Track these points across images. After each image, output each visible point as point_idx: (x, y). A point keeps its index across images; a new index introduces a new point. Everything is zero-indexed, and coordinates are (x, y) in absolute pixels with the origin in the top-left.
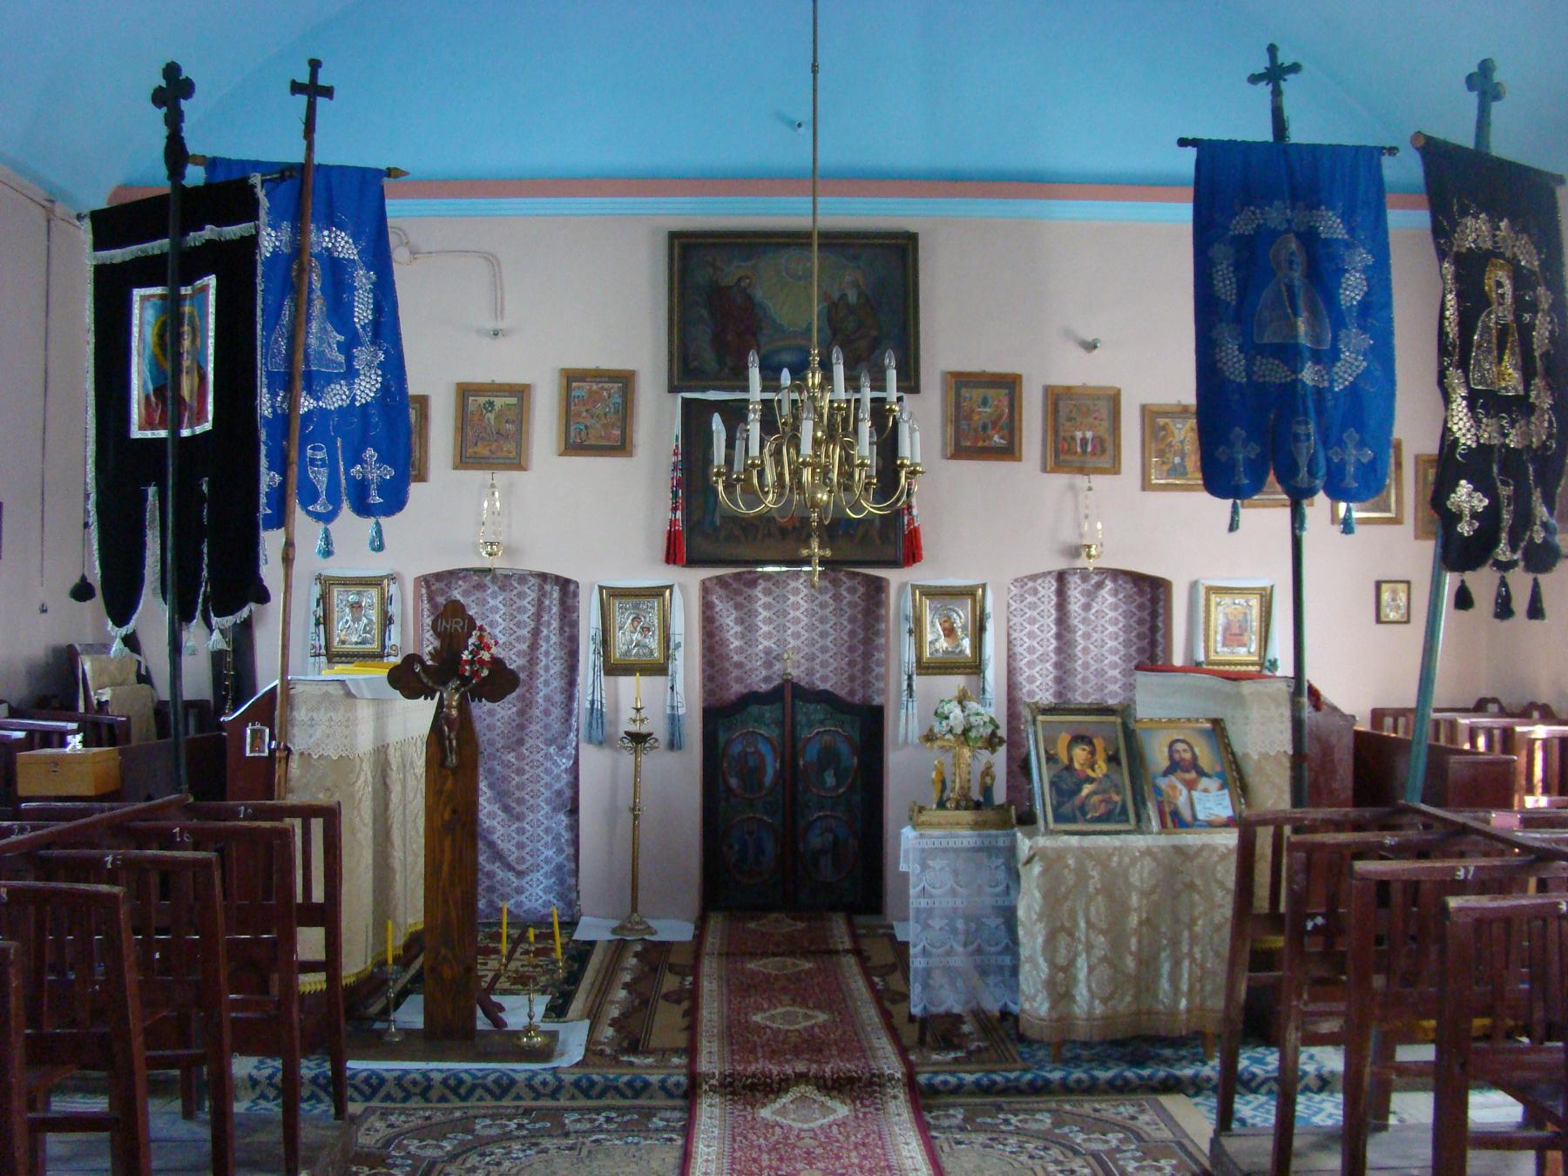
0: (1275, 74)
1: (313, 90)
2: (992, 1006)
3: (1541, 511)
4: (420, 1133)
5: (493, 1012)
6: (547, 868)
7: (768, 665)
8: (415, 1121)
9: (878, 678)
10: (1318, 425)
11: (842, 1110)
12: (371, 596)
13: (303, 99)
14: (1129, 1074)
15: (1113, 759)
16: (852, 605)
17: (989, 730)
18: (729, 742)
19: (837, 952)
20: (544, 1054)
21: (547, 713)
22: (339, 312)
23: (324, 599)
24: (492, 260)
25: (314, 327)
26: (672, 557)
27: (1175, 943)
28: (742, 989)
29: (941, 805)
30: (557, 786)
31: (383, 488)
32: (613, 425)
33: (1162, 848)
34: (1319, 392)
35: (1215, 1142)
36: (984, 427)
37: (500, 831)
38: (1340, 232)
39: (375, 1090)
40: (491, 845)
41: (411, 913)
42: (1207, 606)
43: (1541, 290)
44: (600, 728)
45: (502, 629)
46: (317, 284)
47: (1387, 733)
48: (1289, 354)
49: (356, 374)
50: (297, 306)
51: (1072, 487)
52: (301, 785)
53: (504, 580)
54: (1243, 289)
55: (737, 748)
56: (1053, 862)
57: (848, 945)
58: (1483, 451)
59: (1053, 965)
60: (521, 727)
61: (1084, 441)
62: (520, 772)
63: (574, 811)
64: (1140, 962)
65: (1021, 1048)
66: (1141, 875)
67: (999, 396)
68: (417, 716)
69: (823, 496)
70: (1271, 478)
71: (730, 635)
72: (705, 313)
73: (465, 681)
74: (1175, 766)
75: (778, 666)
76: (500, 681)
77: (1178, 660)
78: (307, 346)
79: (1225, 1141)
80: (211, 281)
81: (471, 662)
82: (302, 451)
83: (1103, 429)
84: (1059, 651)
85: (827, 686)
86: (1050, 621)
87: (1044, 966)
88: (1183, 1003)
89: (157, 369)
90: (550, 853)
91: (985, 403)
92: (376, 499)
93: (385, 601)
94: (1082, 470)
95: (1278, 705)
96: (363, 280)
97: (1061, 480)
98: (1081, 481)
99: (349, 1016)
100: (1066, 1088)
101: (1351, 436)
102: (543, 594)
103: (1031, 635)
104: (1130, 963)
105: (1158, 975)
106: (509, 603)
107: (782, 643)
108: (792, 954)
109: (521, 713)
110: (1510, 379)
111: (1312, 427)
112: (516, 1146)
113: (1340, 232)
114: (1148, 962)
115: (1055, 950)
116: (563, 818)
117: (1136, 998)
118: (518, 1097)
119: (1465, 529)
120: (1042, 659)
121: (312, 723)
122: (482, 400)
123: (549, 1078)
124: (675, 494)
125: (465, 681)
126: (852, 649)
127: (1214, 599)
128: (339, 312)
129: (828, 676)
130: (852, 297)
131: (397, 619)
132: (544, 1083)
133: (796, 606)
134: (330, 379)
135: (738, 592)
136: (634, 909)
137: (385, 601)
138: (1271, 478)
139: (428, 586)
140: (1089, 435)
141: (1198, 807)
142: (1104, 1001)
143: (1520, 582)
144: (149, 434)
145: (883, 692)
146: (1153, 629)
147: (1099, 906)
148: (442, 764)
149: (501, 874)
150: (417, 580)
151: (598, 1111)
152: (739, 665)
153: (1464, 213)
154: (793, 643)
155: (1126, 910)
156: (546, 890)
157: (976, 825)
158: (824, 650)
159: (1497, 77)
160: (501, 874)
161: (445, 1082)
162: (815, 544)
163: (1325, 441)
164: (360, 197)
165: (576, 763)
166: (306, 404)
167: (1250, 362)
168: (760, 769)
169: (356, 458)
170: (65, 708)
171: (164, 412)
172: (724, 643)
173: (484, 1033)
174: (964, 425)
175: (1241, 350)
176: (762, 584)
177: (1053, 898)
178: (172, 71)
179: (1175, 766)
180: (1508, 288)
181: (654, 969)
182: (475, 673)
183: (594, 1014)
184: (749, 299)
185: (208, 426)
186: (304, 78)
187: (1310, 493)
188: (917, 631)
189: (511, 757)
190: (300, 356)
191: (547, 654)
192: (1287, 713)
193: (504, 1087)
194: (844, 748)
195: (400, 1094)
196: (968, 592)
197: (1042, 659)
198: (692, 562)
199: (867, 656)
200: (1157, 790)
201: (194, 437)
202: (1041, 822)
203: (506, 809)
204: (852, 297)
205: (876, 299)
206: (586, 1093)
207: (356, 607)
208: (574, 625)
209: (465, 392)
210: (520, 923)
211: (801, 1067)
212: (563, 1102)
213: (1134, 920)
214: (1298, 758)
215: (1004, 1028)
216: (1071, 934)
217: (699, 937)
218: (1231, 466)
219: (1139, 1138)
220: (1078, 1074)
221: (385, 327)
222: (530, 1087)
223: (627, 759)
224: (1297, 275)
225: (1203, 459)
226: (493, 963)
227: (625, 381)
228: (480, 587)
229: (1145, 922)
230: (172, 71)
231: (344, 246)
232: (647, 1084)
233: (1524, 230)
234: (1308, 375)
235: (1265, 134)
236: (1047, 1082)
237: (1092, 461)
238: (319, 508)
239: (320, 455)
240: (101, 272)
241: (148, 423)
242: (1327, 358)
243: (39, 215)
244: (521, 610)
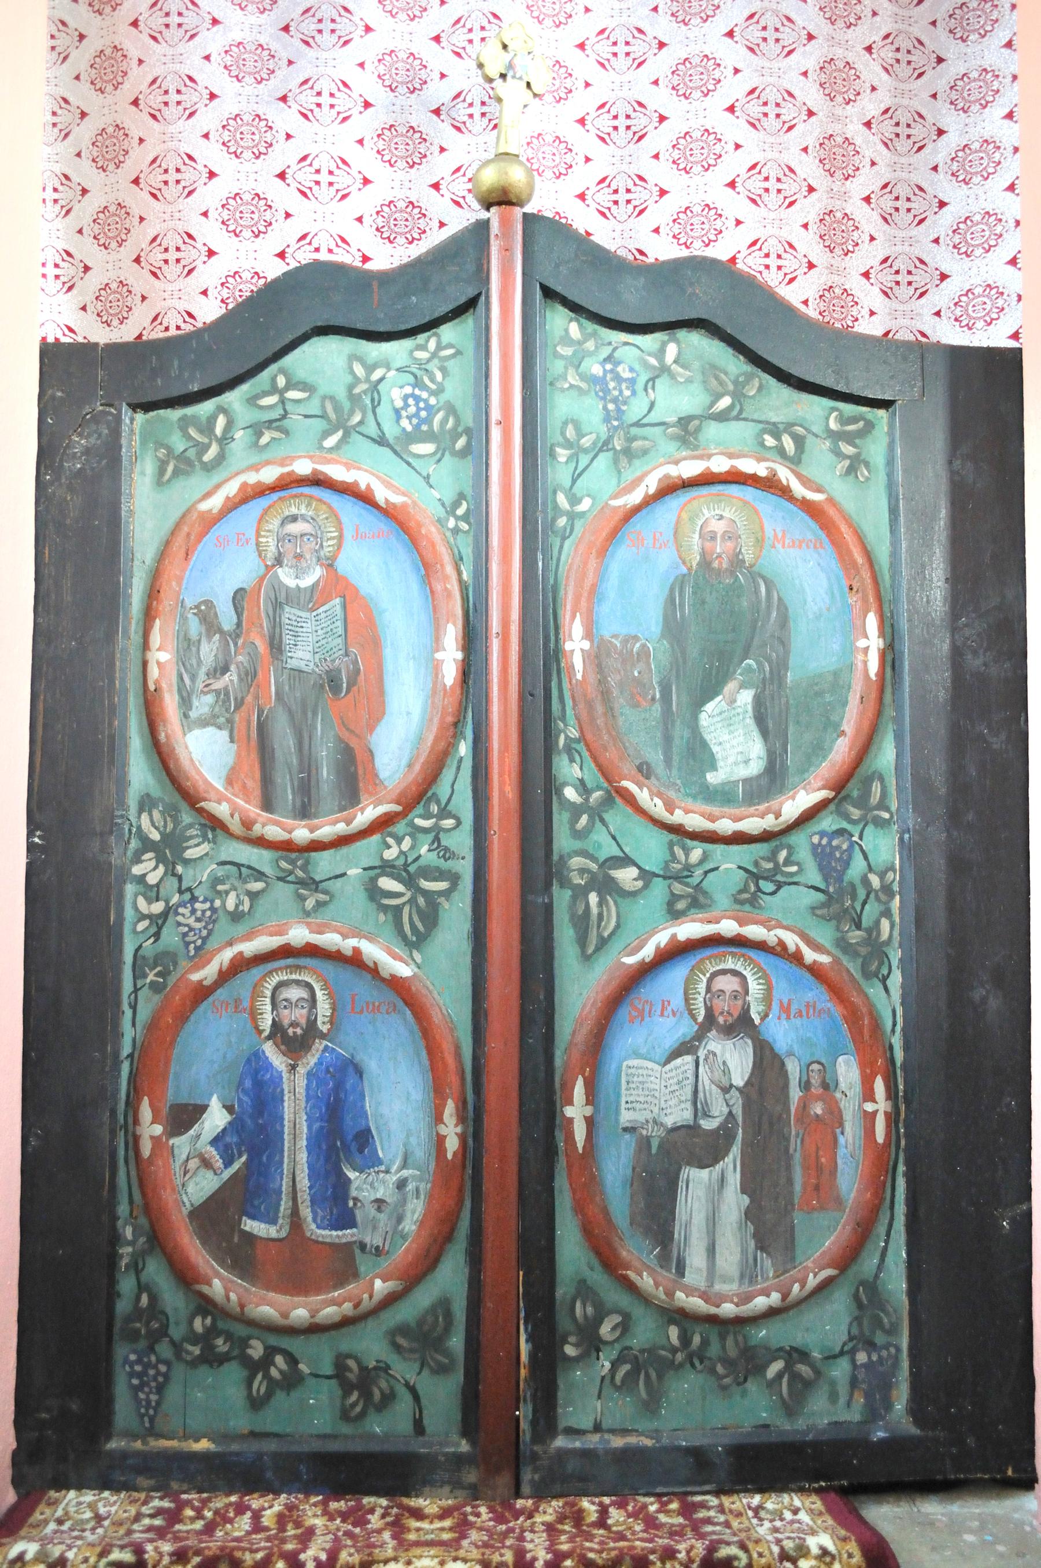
18: (190, 532)
55: (222, 571)
194: (805, 575)
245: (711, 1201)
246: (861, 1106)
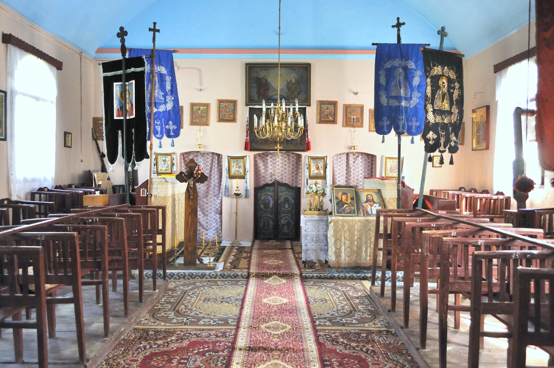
0: (399, 25)
1: (154, 30)
2: (323, 259)
3: (454, 138)
4: (183, 285)
5: (201, 261)
6: (214, 228)
7: (271, 177)
8: (181, 283)
9: (300, 180)
10: (406, 117)
11: (284, 281)
12: (169, 158)
13: (152, 33)
14: (354, 275)
15: (352, 199)
16: (293, 161)
17: (322, 191)
18: (261, 196)
19: (287, 249)
20: (213, 268)
21: (214, 188)
22: (162, 87)
23: (156, 159)
24: (199, 70)
25: (156, 91)
26: (246, 149)
27: (366, 243)
28: (262, 256)
29: (310, 210)
30: (217, 207)
31: (174, 131)
32: (231, 114)
33: (363, 220)
34: (406, 108)
35: (371, 288)
36: (328, 115)
37: (202, 219)
39: (172, 277)
40: (200, 222)
41: (181, 237)
42: (386, 162)
43: (456, 84)
45: (203, 166)
46: (157, 80)
47: (434, 195)
49: (167, 103)
50: (152, 86)
51: (350, 131)
52: (154, 202)
53: (203, 154)
54: (387, 83)
55: (263, 198)
56: (336, 222)
57: (290, 247)
58: (437, 124)
59: (336, 248)
60: (207, 192)
61: (354, 119)
64: (357, 248)
65: (329, 269)
66: (357, 227)
67: (332, 107)
68: (183, 187)
69: (280, 134)
70: (393, 129)
71: (261, 169)
72: (255, 85)
73: (195, 178)
74: (368, 201)
75: (273, 177)
76: (203, 178)
77: (378, 176)
78: (155, 96)
79: (373, 288)
80: (134, 81)
81: (196, 174)
82: (154, 122)
83: (359, 116)
84: (347, 174)
85: (286, 182)
86: (344, 166)
87: (334, 248)
88: (368, 258)
89: (120, 103)
90: (214, 224)
91: (328, 109)
92: (172, 134)
93: (172, 159)
94: (353, 126)
95: (394, 186)
96: (168, 79)
97: (348, 129)
98: (352, 129)
99: (165, 260)
100: (339, 278)
101: (414, 119)
102: (213, 158)
104: (355, 248)
106: (204, 160)
107: (275, 171)
108: (275, 249)
109: (207, 188)
110: (446, 106)
111: (404, 117)
112: (206, 288)
115: (337, 244)
116: (218, 216)
117: (356, 256)
118: (207, 278)
119: (431, 142)
121: (157, 188)
122: (197, 107)
123: (214, 273)
124: (247, 132)
125: (195, 178)
126: (293, 173)
127: (388, 160)
128: (162, 87)
129: (286, 180)
130: (293, 81)
131: (175, 164)
132: (213, 275)
133: (278, 162)
134: (160, 104)
135: (263, 158)
136: (236, 238)
137: (172, 159)
138: (393, 129)
139: (183, 156)
140: (355, 117)
142: (349, 257)
143: (447, 156)
144: (119, 118)
145: (300, 184)
146: (372, 168)
147: (347, 235)
148: (189, 198)
149: (202, 230)
151: (226, 281)
152: (264, 177)
153: (434, 65)
154: (277, 171)
155: (354, 235)
156: (214, 234)
157: (319, 215)
158: (285, 173)
159: (446, 31)
160: (202, 230)
161: (189, 275)
162: (278, 146)
164: (166, 57)
165: (222, 201)
166: (155, 110)
168: (269, 203)
170: (90, 186)
171: (122, 113)
172: (259, 171)
173: (198, 264)
174: (322, 114)
175: (386, 97)
176: (270, 156)
177: (336, 231)
178: (122, 29)
179: (368, 201)
180: (446, 83)
181: (241, 252)
182: (197, 176)
183: (225, 261)
184: (266, 81)
185: (134, 116)
186: (152, 27)
187: (403, 133)
188: (309, 168)
189: (205, 200)
190: (153, 98)
191: (214, 173)
192: (396, 188)
193: (203, 276)
194: (290, 198)
195: (178, 278)
196: (323, 158)
198: (251, 150)
199: (297, 174)
200: (363, 206)
201: (130, 119)
202: (333, 214)
203: (203, 213)
204: (293, 81)
205: (300, 80)
206: (223, 277)
207: (164, 161)
208: (221, 166)
209: (193, 105)
210: (207, 243)
211: (275, 272)
212: (217, 279)
213: (356, 237)
214: (399, 199)
215: (326, 265)
216: (340, 240)
217: (252, 246)
218: (383, 127)
219: (355, 288)
220: (342, 275)
221: (174, 91)
222: (209, 276)
223: (234, 200)
224: (401, 78)
225: (375, 124)
226: (200, 251)
227: (234, 102)
228: (197, 156)
229: (359, 238)
230: (122, 29)
231: (163, 70)
232: (238, 275)
233: (452, 69)
234: (403, 103)
235: (395, 41)
236: (334, 276)
238: (158, 136)
239: (158, 123)
240: (105, 78)
241: (118, 116)
242: (409, 99)
243: (78, 56)
244: (207, 162)
245: (286, 227)
246: (293, 223)
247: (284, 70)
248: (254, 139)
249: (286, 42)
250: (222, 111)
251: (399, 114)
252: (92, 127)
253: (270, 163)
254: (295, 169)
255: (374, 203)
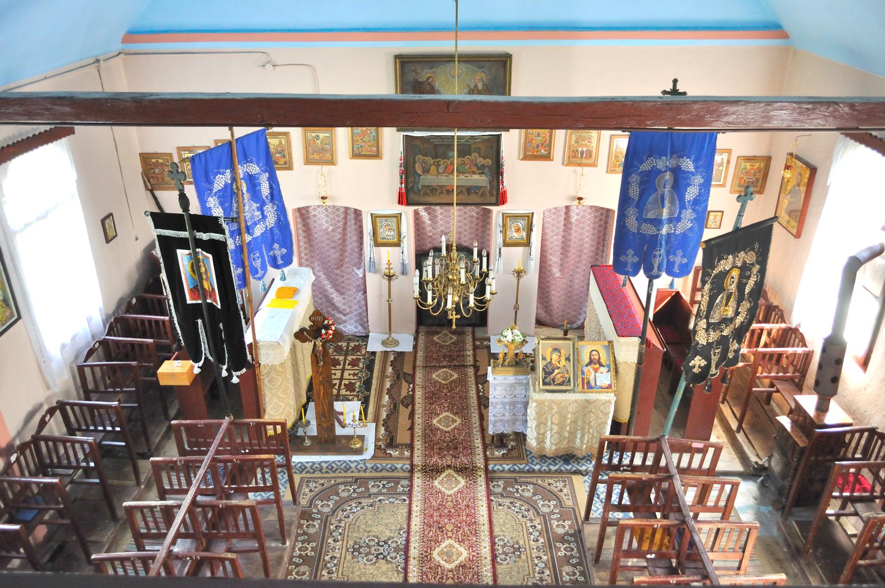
6: (356, 313)
15: (568, 359)
22: (255, 193)
26: (400, 202)
27: (583, 429)
32: (373, 145)
36: (538, 146)
38: (691, 168)
44: (374, 266)
48: (657, 222)
51: (575, 171)
54: (642, 194)
59: (538, 433)
60: (341, 260)
61: (582, 152)
62: (342, 277)
63: (365, 292)
64: (569, 432)
70: (642, 271)
74: (591, 362)
82: (249, 257)
92: (280, 262)
94: (580, 165)
97: (571, 169)
98: (579, 169)
101: (680, 253)
103: (553, 231)
104: (567, 434)
105: (576, 437)
109: (341, 255)
113: (691, 168)
114: (573, 433)
120: (557, 234)
128: (255, 193)
138: (642, 271)
140: (585, 149)
141: (598, 380)
142: (556, 445)
144: (194, 302)
147: (556, 419)
150: (294, 211)
152: (430, 237)
155: (566, 419)
163: (668, 253)
166: (248, 238)
167: (640, 225)
169: (271, 248)
175: (637, 220)
177: (539, 415)
183: (376, 420)
189: (338, 272)
197: (557, 234)
198: (408, 204)
199: (483, 232)
203: (337, 290)
208: (361, 227)
221: (276, 195)
231: (254, 169)
232: (396, 468)
237: (584, 161)
238: (259, 275)
242: (674, 220)
247: (464, 66)
248: (412, 187)
249: (467, 15)
250: (357, 141)
251: (656, 247)
252: (141, 170)
253: (441, 217)
254: (480, 230)
255: (601, 365)
